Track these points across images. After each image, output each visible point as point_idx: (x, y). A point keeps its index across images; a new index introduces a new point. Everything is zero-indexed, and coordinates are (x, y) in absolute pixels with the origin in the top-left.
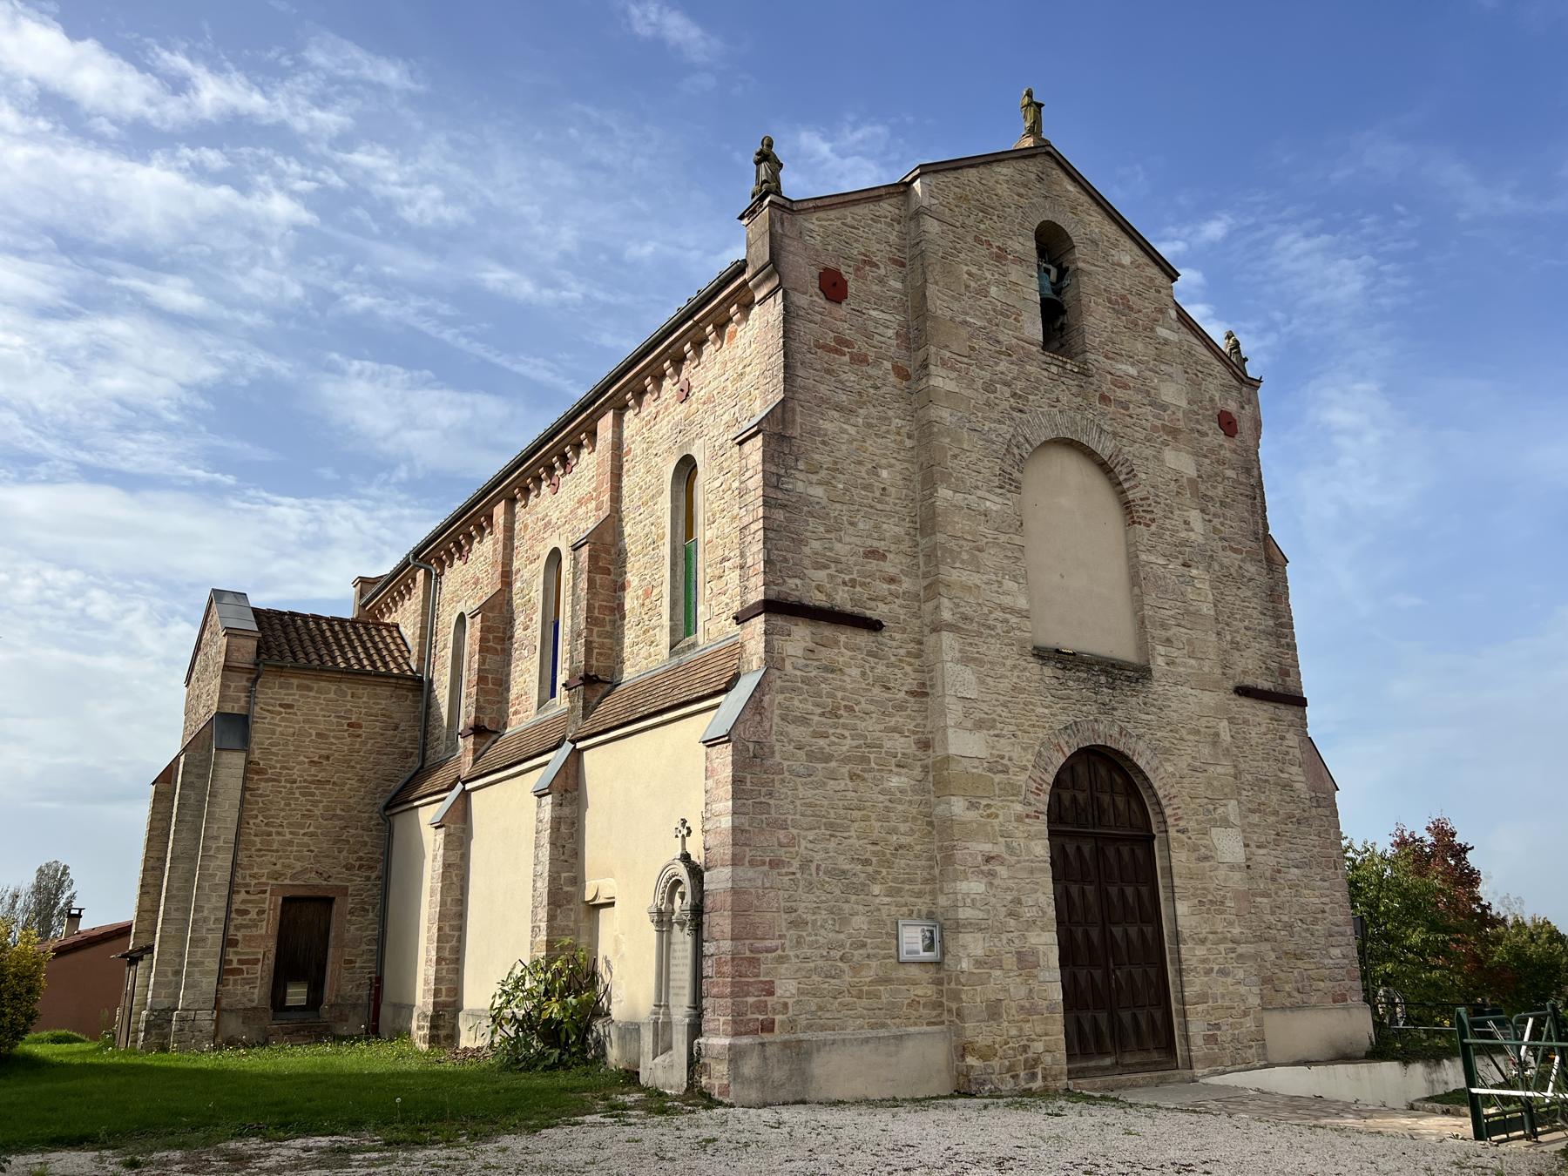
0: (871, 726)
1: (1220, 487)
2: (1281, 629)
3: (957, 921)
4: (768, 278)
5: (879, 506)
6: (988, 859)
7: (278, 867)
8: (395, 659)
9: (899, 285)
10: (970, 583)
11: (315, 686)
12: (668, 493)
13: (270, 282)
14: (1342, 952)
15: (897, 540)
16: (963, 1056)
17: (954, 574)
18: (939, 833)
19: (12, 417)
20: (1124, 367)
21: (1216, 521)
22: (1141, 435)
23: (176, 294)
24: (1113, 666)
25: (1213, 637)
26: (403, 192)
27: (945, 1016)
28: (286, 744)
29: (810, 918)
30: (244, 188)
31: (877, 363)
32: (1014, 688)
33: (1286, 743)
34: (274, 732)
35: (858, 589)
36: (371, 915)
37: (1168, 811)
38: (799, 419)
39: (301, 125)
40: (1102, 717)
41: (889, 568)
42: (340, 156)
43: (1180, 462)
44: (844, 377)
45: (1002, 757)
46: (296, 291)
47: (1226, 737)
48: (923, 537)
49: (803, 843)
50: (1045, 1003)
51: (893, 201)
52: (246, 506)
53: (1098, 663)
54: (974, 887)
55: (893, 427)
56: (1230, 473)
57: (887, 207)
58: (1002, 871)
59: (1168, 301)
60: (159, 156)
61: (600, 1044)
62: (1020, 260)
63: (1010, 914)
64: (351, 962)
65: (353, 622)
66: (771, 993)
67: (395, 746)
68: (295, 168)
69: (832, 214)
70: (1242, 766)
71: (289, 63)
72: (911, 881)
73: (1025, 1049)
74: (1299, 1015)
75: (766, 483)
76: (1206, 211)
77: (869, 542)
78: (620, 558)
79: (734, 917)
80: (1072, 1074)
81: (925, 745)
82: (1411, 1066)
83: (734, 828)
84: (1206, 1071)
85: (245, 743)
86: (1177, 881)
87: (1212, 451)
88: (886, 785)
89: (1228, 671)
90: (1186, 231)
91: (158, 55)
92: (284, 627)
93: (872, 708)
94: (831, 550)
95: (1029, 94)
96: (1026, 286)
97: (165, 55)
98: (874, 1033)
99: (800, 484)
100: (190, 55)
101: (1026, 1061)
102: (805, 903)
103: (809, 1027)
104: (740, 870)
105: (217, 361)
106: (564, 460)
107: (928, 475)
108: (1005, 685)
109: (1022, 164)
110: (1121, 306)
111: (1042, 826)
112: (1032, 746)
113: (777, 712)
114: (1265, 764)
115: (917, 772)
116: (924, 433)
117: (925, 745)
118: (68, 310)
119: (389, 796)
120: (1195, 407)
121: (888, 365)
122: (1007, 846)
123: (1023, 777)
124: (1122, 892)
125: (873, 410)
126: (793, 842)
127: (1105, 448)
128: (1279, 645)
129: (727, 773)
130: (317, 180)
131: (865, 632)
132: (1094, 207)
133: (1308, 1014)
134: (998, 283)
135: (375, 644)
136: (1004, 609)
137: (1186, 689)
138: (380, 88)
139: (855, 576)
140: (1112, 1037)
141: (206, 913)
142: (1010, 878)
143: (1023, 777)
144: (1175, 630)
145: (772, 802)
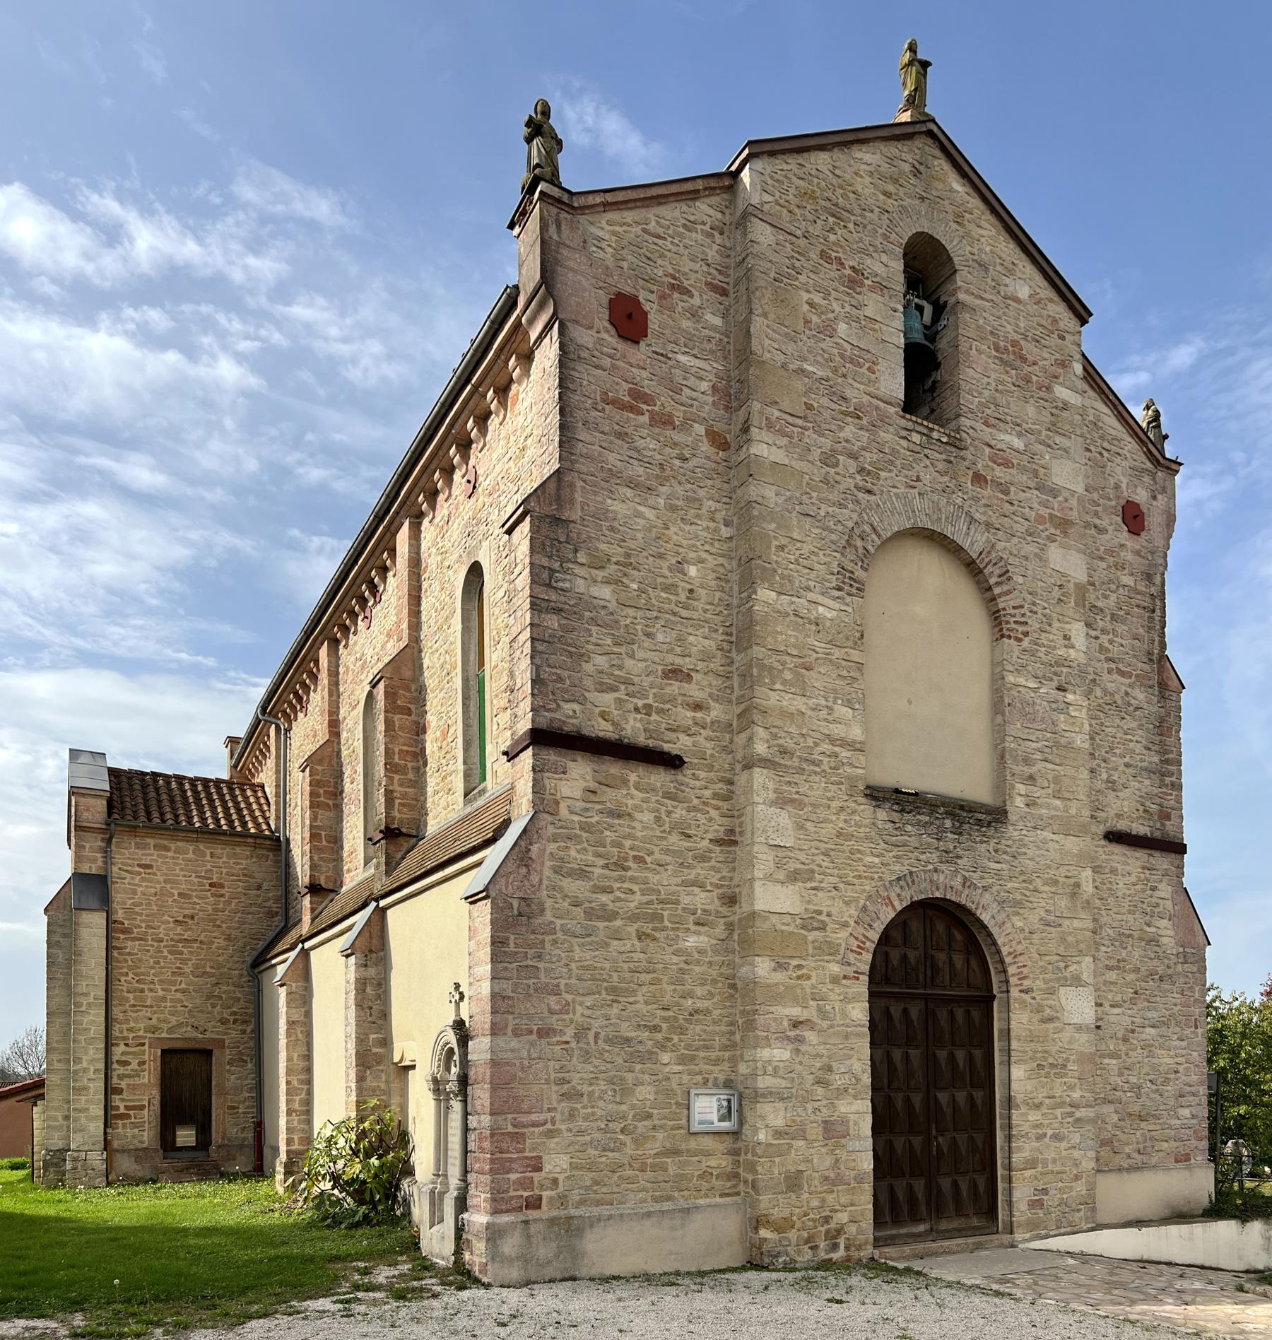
0: (666, 880)
1: (1113, 597)
2: (1166, 768)
3: (755, 1090)
4: (541, 306)
5: (684, 613)
6: (796, 1024)
7: (154, 1021)
8: (254, 819)
9: (718, 321)
10: (792, 709)
11: (173, 846)
12: (459, 611)
13: (224, 454)
14: (1192, 1113)
15: (706, 657)
16: (756, 1229)
17: (772, 698)
18: (743, 997)
19: (10, 605)
20: (1007, 438)
21: (1104, 639)
22: (1021, 527)
23: (142, 473)
24: (962, 808)
25: (1085, 774)
26: (344, 349)
27: (741, 1187)
28: (149, 904)
29: (586, 1089)
30: (191, 353)
31: (686, 426)
32: (839, 834)
33: (1157, 894)
34: (135, 893)
35: (654, 717)
36: (250, 1066)
37: (1011, 970)
38: (579, 498)
39: (237, 276)
40: (943, 867)
41: (694, 691)
42: (279, 309)
43: (1068, 562)
44: (640, 443)
45: (820, 913)
46: (251, 465)
47: (1088, 888)
48: (739, 652)
49: (579, 1009)
50: (853, 1173)
51: (715, 200)
52: (228, 687)
53: (943, 805)
54: (780, 1053)
55: (704, 511)
56: (1127, 580)
57: (705, 210)
58: (811, 1036)
59: (1073, 350)
60: (104, 318)
61: (406, 1203)
62: (881, 287)
63: (819, 1082)
64: (234, 1108)
65: (229, 784)
66: (540, 1169)
67: (259, 906)
68: (237, 326)
69: (630, 216)
70: (1104, 920)
71: (218, 201)
72: (707, 1048)
73: (827, 1220)
74: (1136, 1176)
75: (535, 580)
76: (1176, 334)
77: (670, 658)
78: (420, 696)
79: (494, 1090)
80: (877, 1243)
81: (731, 900)
82: (1248, 1224)
83: (494, 996)
84: (1028, 1235)
85: (105, 902)
86: (1014, 1044)
87: (1110, 552)
88: (682, 945)
89: (1100, 814)
90: (1152, 358)
91: (87, 198)
92: (144, 787)
93: (668, 859)
94: (620, 667)
95: (912, 48)
96: (887, 325)
97: (95, 198)
98: (657, 1207)
99: (580, 582)
100: (120, 196)
101: (827, 1232)
102: (580, 1075)
103: (582, 1202)
104: (501, 1041)
105: (185, 542)
106: (373, 589)
107: (746, 570)
108: (828, 830)
109: (893, 149)
110: (1011, 355)
111: (862, 987)
112: (856, 900)
113: (548, 864)
114: (1130, 918)
115: (720, 930)
116: (743, 516)
117: (731, 900)
118: (45, 494)
119: (255, 954)
120: (1095, 496)
121: (700, 429)
122: (819, 1009)
123: (843, 934)
124: (952, 1057)
125: (678, 489)
126: (566, 1008)
127: (974, 542)
128: (1162, 784)
129: (486, 933)
130: (257, 338)
131: (661, 769)
132: (988, 216)
133: (1147, 1175)
134: (849, 319)
135: (236, 804)
136: (833, 741)
137: (1047, 834)
138: (312, 227)
139: (650, 701)
140: (928, 1204)
141: (85, 1064)
142: (820, 1043)
143: (843, 934)
144: (1041, 765)
145: (541, 965)
